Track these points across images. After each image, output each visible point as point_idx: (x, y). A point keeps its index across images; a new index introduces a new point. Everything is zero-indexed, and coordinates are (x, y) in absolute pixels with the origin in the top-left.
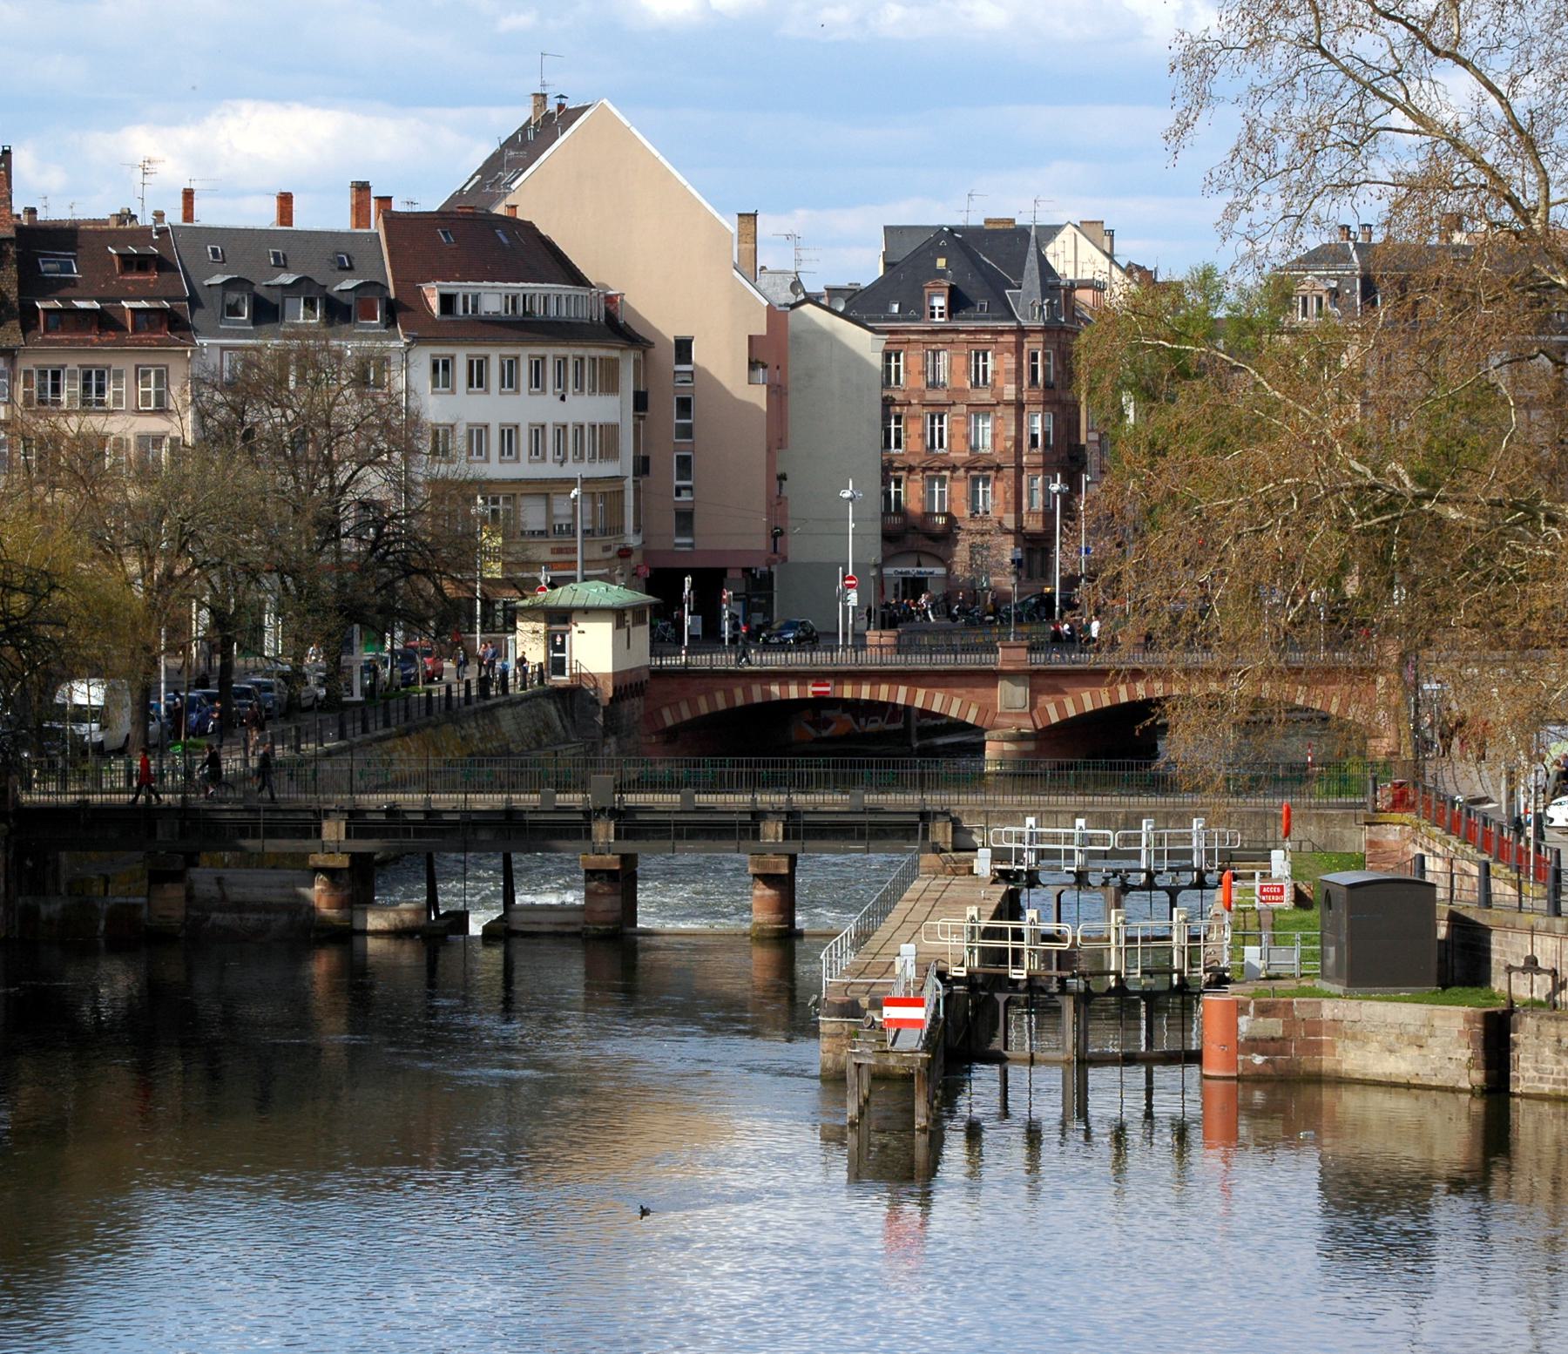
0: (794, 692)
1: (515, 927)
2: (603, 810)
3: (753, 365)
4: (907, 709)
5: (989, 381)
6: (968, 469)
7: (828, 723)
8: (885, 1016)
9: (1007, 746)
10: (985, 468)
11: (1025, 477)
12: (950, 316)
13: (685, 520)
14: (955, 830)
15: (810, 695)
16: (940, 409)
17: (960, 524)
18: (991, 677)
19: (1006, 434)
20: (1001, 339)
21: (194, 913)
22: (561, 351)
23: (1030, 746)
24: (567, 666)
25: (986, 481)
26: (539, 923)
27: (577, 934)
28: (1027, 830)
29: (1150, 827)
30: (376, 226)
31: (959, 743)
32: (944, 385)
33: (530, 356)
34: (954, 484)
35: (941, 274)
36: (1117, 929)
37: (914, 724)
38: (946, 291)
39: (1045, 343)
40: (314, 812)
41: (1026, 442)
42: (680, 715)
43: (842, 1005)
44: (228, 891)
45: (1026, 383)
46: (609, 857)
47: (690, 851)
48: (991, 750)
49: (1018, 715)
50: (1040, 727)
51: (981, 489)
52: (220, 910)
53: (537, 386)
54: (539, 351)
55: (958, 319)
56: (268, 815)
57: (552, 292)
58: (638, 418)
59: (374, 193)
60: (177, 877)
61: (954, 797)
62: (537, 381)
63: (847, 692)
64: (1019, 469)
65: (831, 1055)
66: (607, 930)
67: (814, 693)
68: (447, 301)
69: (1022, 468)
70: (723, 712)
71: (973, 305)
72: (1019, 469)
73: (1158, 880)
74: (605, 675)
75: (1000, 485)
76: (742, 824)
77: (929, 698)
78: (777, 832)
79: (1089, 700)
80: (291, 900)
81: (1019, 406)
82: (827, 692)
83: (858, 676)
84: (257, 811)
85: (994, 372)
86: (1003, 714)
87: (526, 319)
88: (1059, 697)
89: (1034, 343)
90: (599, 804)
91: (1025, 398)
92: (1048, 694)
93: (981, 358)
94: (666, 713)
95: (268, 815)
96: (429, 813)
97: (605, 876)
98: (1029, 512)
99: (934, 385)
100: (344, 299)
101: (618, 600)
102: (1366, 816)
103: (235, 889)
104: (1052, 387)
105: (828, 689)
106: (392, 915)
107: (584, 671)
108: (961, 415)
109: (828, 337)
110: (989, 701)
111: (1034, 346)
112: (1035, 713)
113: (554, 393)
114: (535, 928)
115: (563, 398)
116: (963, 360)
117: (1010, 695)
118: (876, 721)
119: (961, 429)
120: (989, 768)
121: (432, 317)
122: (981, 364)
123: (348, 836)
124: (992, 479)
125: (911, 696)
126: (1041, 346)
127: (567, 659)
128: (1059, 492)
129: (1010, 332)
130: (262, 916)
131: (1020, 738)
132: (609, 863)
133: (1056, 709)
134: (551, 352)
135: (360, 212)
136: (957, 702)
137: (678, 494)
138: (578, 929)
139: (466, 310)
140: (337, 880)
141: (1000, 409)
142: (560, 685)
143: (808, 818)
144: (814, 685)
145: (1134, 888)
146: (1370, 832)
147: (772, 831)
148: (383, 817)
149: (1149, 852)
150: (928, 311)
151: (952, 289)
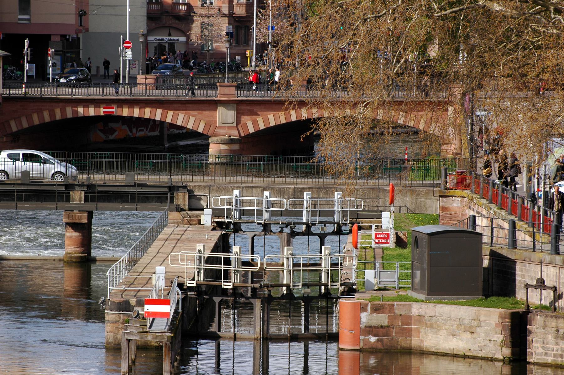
0: (92, 112)
7: (113, 131)
8: (146, 310)
9: (223, 147)
14: (190, 198)
15: (102, 114)
17: (195, 10)
18: (213, 104)
23: (236, 147)
28: (234, 198)
36: (288, 258)
37: (166, 132)
43: (119, 303)
48: (213, 149)
49: (229, 128)
50: (243, 135)
63: (125, 112)
65: (112, 334)
67: (104, 112)
73: (314, 229)
76: (59, 192)
77: (175, 117)
78: (81, 197)
82: (113, 112)
83: (131, 103)
86: (220, 127)
88: (254, 117)
92: (248, 115)
94: (13, 124)
105: (113, 110)
112: (240, 127)
118: (143, 130)
125: (164, 115)
131: (231, 141)
136: (192, 120)
144: (104, 108)
145: (298, 234)
146: (443, 201)
147: (78, 196)
149: (308, 212)
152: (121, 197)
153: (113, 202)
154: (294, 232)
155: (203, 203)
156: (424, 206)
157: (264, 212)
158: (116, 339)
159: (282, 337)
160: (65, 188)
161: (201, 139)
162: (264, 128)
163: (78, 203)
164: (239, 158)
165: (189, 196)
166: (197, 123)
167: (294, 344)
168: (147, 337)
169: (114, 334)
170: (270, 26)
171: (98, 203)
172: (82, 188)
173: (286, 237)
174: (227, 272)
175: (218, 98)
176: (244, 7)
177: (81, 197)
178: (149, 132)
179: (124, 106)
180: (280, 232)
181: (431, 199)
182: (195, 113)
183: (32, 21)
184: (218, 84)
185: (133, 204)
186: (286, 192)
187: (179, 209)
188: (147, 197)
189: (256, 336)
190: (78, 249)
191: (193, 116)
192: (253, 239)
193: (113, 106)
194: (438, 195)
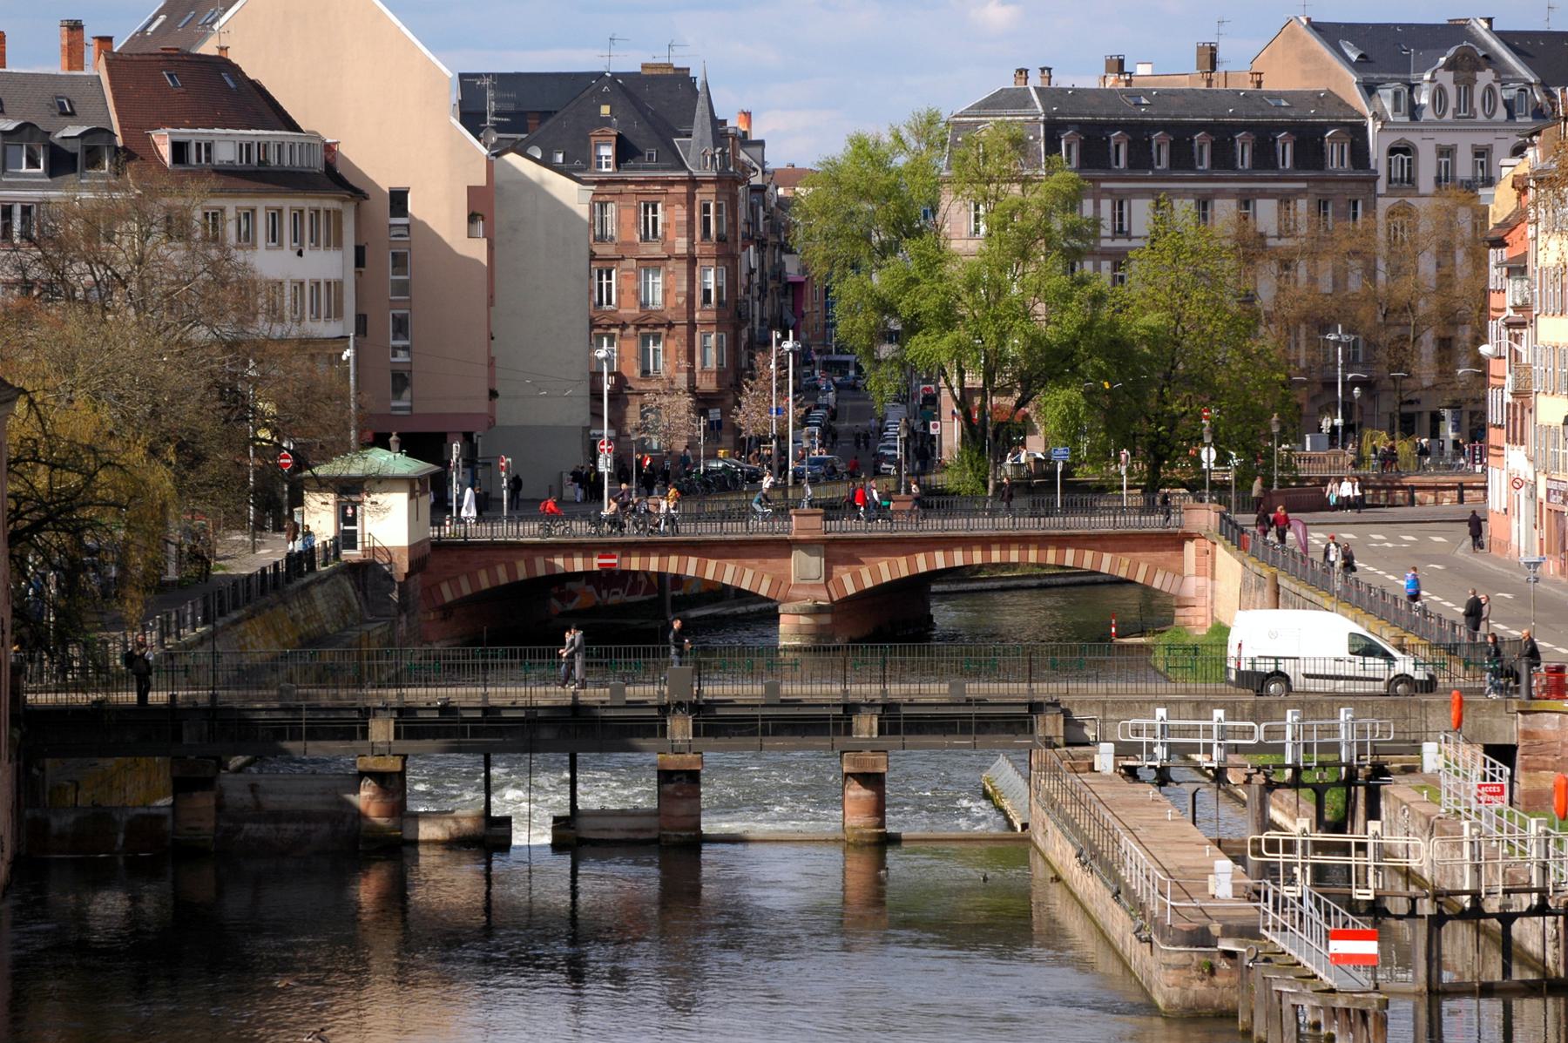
0: (579, 564)
1: (584, 835)
2: (680, 705)
3: (472, 218)
5: (659, 233)
6: (638, 327)
7: (572, 596)
8: (1332, 950)
9: (804, 620)
10: (656, 326)
11: (697, 335)
13: (401, 380)
14: (1066, 722)
15: (596, 568)
16: (608, 264)
17: (630, 384)
18: (784, 547)
20: (671, 190)
21: (225, 824)
22: (298, 203)
23: (826, 619)
24: (359, 539)
25: (657, 338)
26: (609, 830)
27: (657, 841)
28: (1158, 723)
29: (1295, 718)
30: (95, 67)
32: (612, 238)
33: (267, 208)
34: (623, 342)
35: (606, 122)
36: (1472, 843)
37: (670, 593)
38: (614, 139)
40: (359, 710)
41: (699, 298)
42: (460, 590)
43: (1190, 932)
45: (698, 236)
46: (690, 756)
47: (779, 749)
48: (786, 624)
49: (812, 586)
50: (835, 598)
51: (651, 347)
53: (274, 241)
54: (275, 202)
55: (626, 169)
57: (286, 140)
58: (359, 274)
59: (89, 33)
60: (207, 784)
61: (1063, 686)
62: (274, 236)
63: (635, 563)
64: (692, 326)
65: (1177, 989)
66: (691, 836)
67: (600, 565)
68: (179, 149)
70: (505, 586)
71: (641, 154)
72: (692, 326)
73: (1306, 777)
74: (400, 549)
75: (672, 343)
76: (836, 717)
77: (720, 570)
78: (871, 727)
79: (887, 569)
81: (692, 260)
83: (645, 548)
84: (298, 709)
85: (665, 225)
86: (797, 586)
87: (261, 168)
88: (854, 567)
89: (707, 194)
90: (677, 698)
91: (697, 251)
92: (843, 564)
93: (650, 210)
96: (487, 710)
97: (685, 777)
98: (703, 371)
99: (602, 238)
100: (69, 147)
101: (409, 469)
102: (1520, 704)
103: (271, 797)
104: (725, 240)
105: (615, 561)
106: (450, 823)
107: (377, 544)
108: (632, 270)
109: (536, 189)
111: (705, 197)
112: (830, 584)
113: (291, 248)
114: (606, 836)
115: (300, 254)
116: (632, 212)
117: (804, 566)
118: (617, 593)
119: (630, 285)
120: (782, 643)
121: (162, 166)
122: (650, 216)
123: (397, 736)
124: (663, 336)
125: (702, 568)
126: (713, 197)
127: (359, 532)
128: (791, 350)
129: (681, 182)
130: (302, 826)
131: (818, 610)
132: (691, 763)
133: (849, 582)
134: (288, 204)
135: (74, 53)
136: (749, 574)
137: (395, 355)
138: (654, 835)
139: (199, 159)
141: (671, 263)
142: (354, 560)
143: (904, 711)
144: (600, 557)
145: (1279, 785)
146: (1524, 721)
147: (866, 725)
148: (436, 715)
149: (1295, 746)
150: (594, 160)
151: (619, 138)
152: (941, 725)
154: (1271, 782)
155: (1090, 734)
156: (1490, 730)
157: (1215, 746)
158: (1186, 998)
159: (1465, 988)
160: (845, 711)
164: (832, 638)
165: (1065, 721)
167: (1485, 1003)
168: (1334, 1000)
169: (1182, 988)
172: (872, 711)
173: (1258, 792)
174: (1289, 867)
175: (793, 536)
176: (714, 375)
180: (1245, 782)
181: (1501, 717)
182: (755, 562)
183: (416, 410)
184: (792, 511)
186: (1238, 710)
187: (1050, 744)
188: (987, 725)
189: (1417, 988)
191: (751, 567)
192: (1194, 795)
193: (614, 553)
194: (1515, 708)
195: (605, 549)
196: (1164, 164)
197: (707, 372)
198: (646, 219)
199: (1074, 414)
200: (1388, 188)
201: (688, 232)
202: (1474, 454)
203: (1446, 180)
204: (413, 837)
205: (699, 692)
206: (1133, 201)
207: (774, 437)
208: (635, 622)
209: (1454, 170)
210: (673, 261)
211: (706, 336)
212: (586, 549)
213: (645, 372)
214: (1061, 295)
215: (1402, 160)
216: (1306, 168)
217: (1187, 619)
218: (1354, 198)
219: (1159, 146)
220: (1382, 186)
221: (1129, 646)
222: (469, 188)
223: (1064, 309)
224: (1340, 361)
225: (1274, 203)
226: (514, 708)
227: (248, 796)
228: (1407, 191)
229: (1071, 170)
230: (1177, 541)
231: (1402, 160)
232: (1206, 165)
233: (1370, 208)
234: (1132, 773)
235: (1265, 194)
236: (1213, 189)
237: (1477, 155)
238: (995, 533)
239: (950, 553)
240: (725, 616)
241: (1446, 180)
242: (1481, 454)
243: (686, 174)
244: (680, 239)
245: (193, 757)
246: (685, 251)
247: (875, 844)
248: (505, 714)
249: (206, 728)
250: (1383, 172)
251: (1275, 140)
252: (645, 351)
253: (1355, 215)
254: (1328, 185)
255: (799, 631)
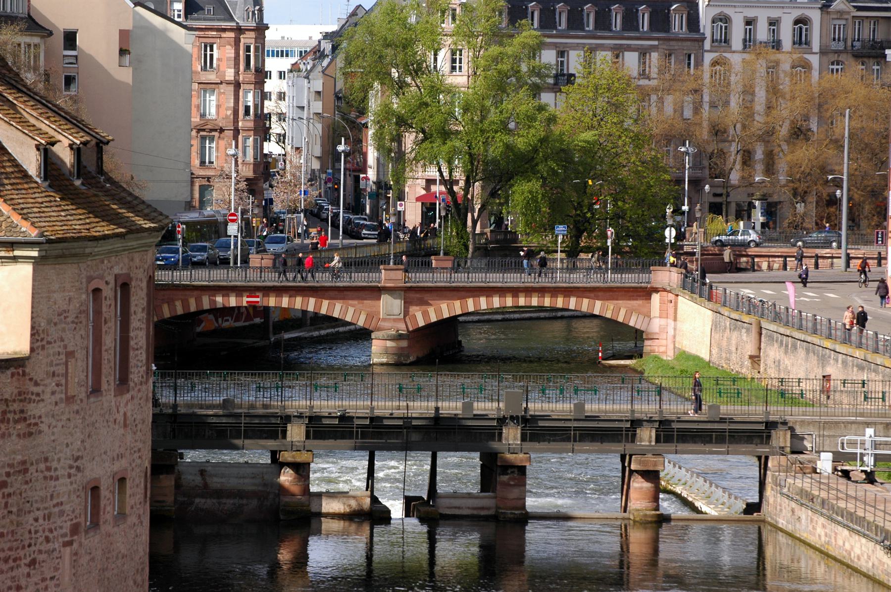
0: (233, 302)
2: (512, 418)
3: (123, 52)
4: (239, 308)
5: (215, 65)
6: (199, 131)
9: (389, 344)
10: (211, 130)
11: (240, 137)
12: (186, 17)
15: (245, 304)
18: (376, 292)
19: (227, 105)
20: (224, 35)
21: (181, 499)
23: (404, 344)
25: (212, 139)
26: (459, 508)
31: (296, 337)
39: (256, 38)
44: (209, 480)
45: (242, 67)
46: (521, 455)
49: (395, 320)
50: (411, 329)
51: (207, 145)
52: (202, 496)
55: (191, 19)
56: (248, 420)
64: (236, 131)
67: (248, 302)
69: (238, 131)
71: (203, 9)
72: (236, 131)
76: (627, 429)
77: (331, 307)
78: (650, 437)
79: (446, 309)
80: (260, 488)
81: (237, 85)
82: (258, 302)
84: (238, 416)
85: (218, 59)
86: (384, 320)
88: (424, 307)
90: (511, 413)
91: (241, 79)
92: (417, 305)
93: (208, 49)
95: (248, 420)
97: (516, 470)
103: (215, 479)
109: (162, 35)
110: (374, 309)
112: (407, 319)
114: (457, 512)
118: (227, 320)
120: (376, 360)
122: (208, 53)
124: (216, 138)
125: (318, 305)
126: (253, 41)
129: (231, 30)
130: (237, 501)
131: (399, 337)
132: (522, 461)
133: (421, 317)
136: (351, 310)
140: (301, 472)
144: (248, 297)
147: (647, 436)
153: (688, 442)
161: (305, 331)
162: (436, 320)
163: (647, 444)
165: (791, 435)
166: (357, 315)
170: (302, 190)
171: (730, 445)
176: (252, 166)
177: (650, 437)
178: (235, 322)
179: (271, 294)
182: (355, 302)
185: (723, 445)
190: (650, 505)
191: (353, 306)
193: (257, 294)
195: (252, 290)
196: (564, 25)
197: (246, 164)
198: (206, 55)
199: (534, 199)
200: (711, 46)
201: (235, 65)
202: (878, 237)
203: (750, 41)
204: (318, 511)
205: (526, 409)
206: (543, 52)
207: (302, 211)
208: (249, 341)
209: (755, 35)
210: (224, 85)
211: (246, 138)
212: (238, 290)
213: (203, 163)
214: (528, 117)
215: (721, 27)
216: (659, 31)
217: (652, 348)
218: (689, 52)
219: (560, 13)
220: (707, 45)
221: (611, 366)
222: (120, 31)
223: (529, 127)
224: (687, 166)
225: (635, 55)
226: (391, 417)
227: (198, 479)
228: (724, 48)
229: (535, 29)
230: (646, 293)
231: (721, 27)
232: (591, 27)
233: (699, 63)
234: (846, 474)
235: (629, 48)
236: (596, 44)
237: (771, 24)
238: (522, 285)
239: (490, 299)
240: (306, 338)
241: (750, 41)
242: (882, 237)
243: (235, 24)
244: (229, 70)
245: (161, 450)
246: (232, 78)
247: (656, 522)
248: (386, 422)
249: (169, 429)
250: (708, 35)
251: (637, 10)
252: (203, 148)
253: (689, 64)
254: (672, 43)
255: (386, 351)
